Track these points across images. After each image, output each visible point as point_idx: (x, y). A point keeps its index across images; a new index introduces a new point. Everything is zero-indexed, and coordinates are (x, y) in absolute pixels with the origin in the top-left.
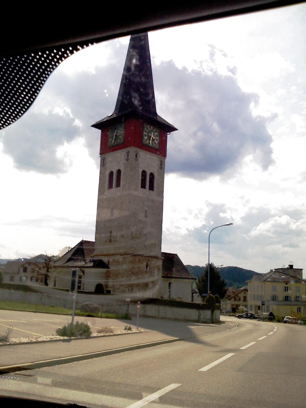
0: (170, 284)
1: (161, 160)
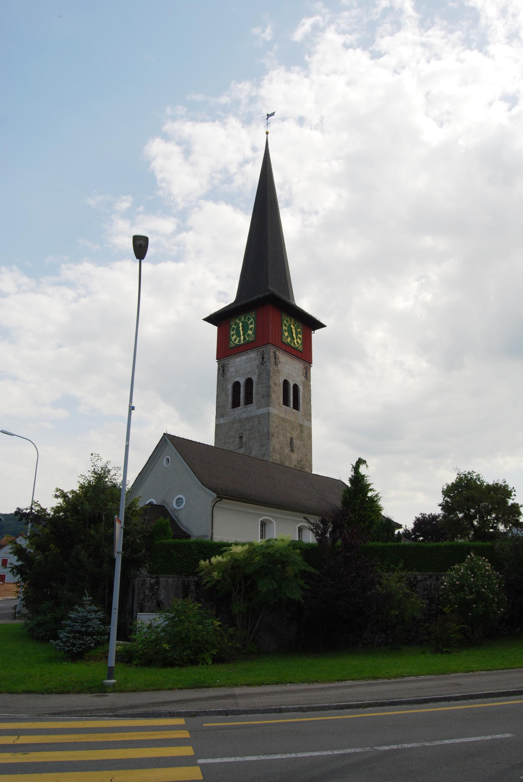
0: (263, 524)
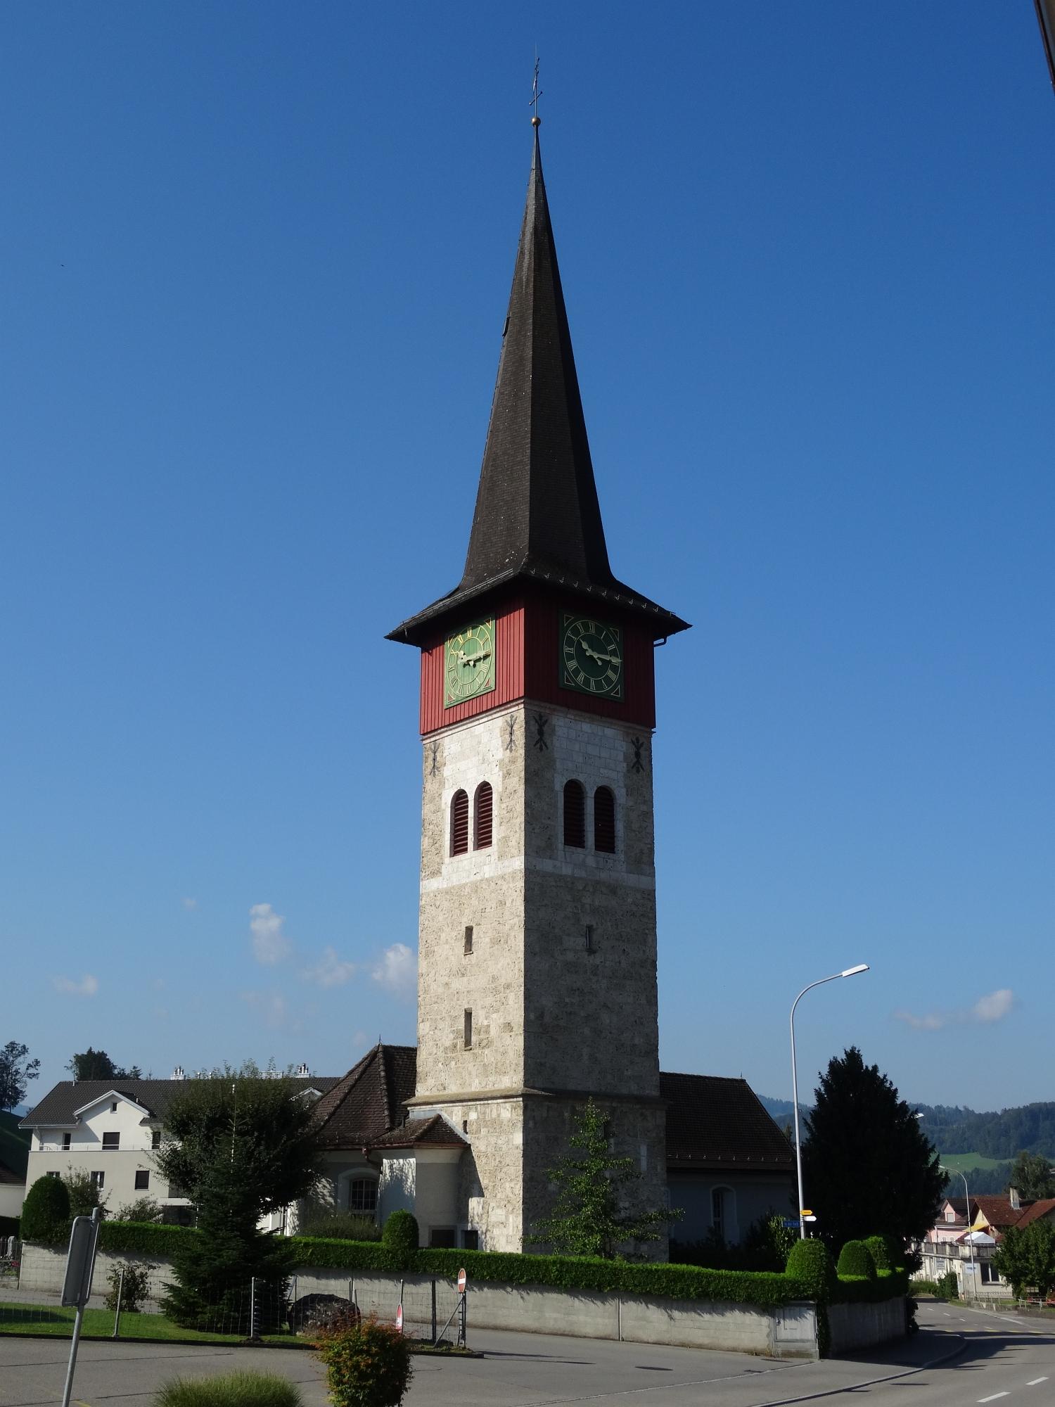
1: (634, 739)
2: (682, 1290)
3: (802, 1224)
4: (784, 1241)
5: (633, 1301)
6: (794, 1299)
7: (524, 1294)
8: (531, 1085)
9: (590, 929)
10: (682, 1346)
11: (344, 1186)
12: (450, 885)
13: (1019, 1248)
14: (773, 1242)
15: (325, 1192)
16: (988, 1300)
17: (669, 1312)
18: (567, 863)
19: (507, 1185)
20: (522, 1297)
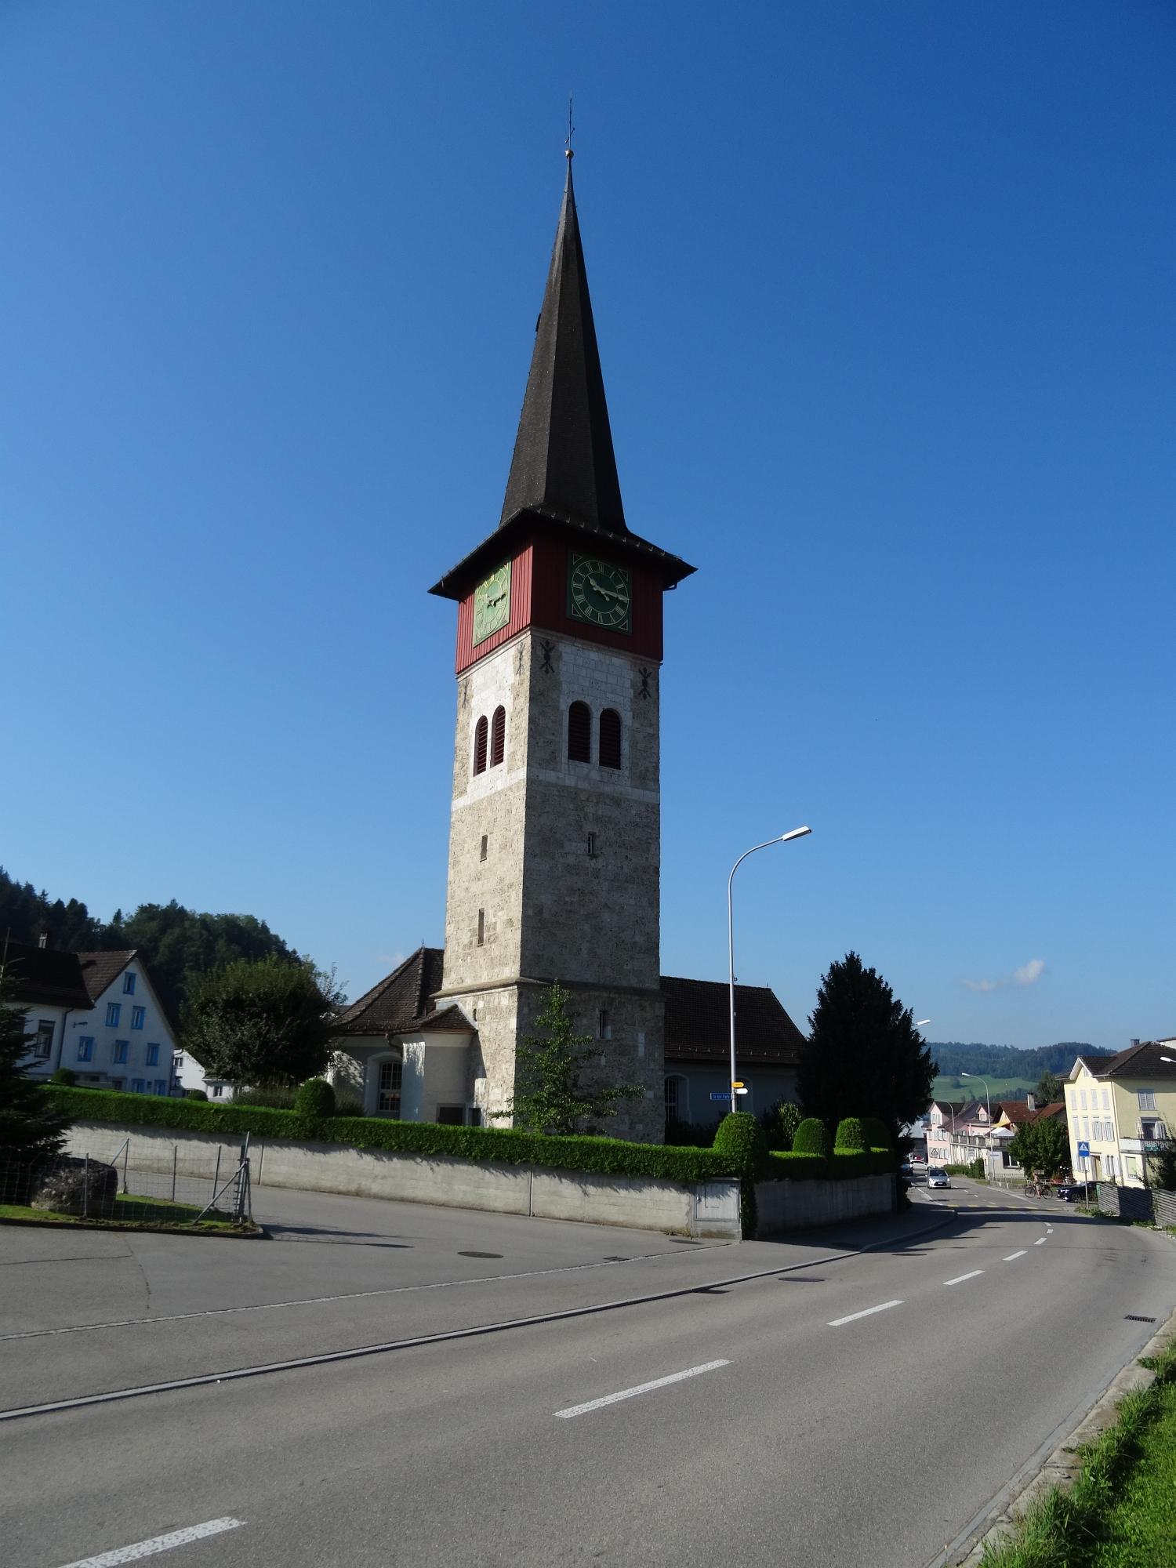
1: (642, 669)
2: (595, 1165)
3: (733, 1097)
4: (792, 1125)
5: (547, 1175)
6: (716, 1175)
7: (434, 1165)
8: (528, 974)
9: (592, 836)
10: (596, 1223)
11: (374, 1069)
12: (472, 802)
13: (1030, 1140)
14: (782, 1125)
15: (356, 1073)
16: (1003, 1180)
17: (584, 1187)
18: (569, 775)
19: (504, 1066)
20: (431, 1169)
